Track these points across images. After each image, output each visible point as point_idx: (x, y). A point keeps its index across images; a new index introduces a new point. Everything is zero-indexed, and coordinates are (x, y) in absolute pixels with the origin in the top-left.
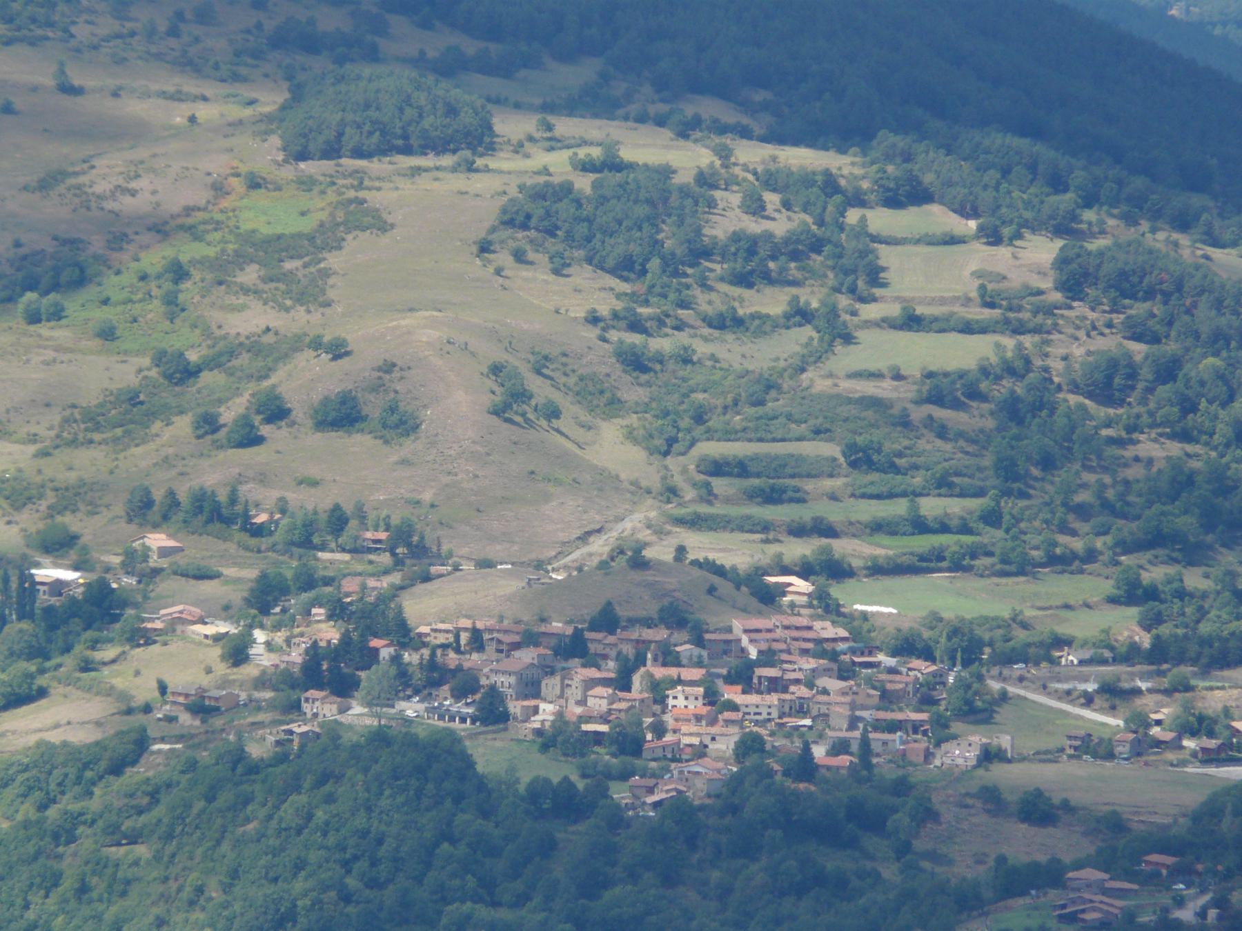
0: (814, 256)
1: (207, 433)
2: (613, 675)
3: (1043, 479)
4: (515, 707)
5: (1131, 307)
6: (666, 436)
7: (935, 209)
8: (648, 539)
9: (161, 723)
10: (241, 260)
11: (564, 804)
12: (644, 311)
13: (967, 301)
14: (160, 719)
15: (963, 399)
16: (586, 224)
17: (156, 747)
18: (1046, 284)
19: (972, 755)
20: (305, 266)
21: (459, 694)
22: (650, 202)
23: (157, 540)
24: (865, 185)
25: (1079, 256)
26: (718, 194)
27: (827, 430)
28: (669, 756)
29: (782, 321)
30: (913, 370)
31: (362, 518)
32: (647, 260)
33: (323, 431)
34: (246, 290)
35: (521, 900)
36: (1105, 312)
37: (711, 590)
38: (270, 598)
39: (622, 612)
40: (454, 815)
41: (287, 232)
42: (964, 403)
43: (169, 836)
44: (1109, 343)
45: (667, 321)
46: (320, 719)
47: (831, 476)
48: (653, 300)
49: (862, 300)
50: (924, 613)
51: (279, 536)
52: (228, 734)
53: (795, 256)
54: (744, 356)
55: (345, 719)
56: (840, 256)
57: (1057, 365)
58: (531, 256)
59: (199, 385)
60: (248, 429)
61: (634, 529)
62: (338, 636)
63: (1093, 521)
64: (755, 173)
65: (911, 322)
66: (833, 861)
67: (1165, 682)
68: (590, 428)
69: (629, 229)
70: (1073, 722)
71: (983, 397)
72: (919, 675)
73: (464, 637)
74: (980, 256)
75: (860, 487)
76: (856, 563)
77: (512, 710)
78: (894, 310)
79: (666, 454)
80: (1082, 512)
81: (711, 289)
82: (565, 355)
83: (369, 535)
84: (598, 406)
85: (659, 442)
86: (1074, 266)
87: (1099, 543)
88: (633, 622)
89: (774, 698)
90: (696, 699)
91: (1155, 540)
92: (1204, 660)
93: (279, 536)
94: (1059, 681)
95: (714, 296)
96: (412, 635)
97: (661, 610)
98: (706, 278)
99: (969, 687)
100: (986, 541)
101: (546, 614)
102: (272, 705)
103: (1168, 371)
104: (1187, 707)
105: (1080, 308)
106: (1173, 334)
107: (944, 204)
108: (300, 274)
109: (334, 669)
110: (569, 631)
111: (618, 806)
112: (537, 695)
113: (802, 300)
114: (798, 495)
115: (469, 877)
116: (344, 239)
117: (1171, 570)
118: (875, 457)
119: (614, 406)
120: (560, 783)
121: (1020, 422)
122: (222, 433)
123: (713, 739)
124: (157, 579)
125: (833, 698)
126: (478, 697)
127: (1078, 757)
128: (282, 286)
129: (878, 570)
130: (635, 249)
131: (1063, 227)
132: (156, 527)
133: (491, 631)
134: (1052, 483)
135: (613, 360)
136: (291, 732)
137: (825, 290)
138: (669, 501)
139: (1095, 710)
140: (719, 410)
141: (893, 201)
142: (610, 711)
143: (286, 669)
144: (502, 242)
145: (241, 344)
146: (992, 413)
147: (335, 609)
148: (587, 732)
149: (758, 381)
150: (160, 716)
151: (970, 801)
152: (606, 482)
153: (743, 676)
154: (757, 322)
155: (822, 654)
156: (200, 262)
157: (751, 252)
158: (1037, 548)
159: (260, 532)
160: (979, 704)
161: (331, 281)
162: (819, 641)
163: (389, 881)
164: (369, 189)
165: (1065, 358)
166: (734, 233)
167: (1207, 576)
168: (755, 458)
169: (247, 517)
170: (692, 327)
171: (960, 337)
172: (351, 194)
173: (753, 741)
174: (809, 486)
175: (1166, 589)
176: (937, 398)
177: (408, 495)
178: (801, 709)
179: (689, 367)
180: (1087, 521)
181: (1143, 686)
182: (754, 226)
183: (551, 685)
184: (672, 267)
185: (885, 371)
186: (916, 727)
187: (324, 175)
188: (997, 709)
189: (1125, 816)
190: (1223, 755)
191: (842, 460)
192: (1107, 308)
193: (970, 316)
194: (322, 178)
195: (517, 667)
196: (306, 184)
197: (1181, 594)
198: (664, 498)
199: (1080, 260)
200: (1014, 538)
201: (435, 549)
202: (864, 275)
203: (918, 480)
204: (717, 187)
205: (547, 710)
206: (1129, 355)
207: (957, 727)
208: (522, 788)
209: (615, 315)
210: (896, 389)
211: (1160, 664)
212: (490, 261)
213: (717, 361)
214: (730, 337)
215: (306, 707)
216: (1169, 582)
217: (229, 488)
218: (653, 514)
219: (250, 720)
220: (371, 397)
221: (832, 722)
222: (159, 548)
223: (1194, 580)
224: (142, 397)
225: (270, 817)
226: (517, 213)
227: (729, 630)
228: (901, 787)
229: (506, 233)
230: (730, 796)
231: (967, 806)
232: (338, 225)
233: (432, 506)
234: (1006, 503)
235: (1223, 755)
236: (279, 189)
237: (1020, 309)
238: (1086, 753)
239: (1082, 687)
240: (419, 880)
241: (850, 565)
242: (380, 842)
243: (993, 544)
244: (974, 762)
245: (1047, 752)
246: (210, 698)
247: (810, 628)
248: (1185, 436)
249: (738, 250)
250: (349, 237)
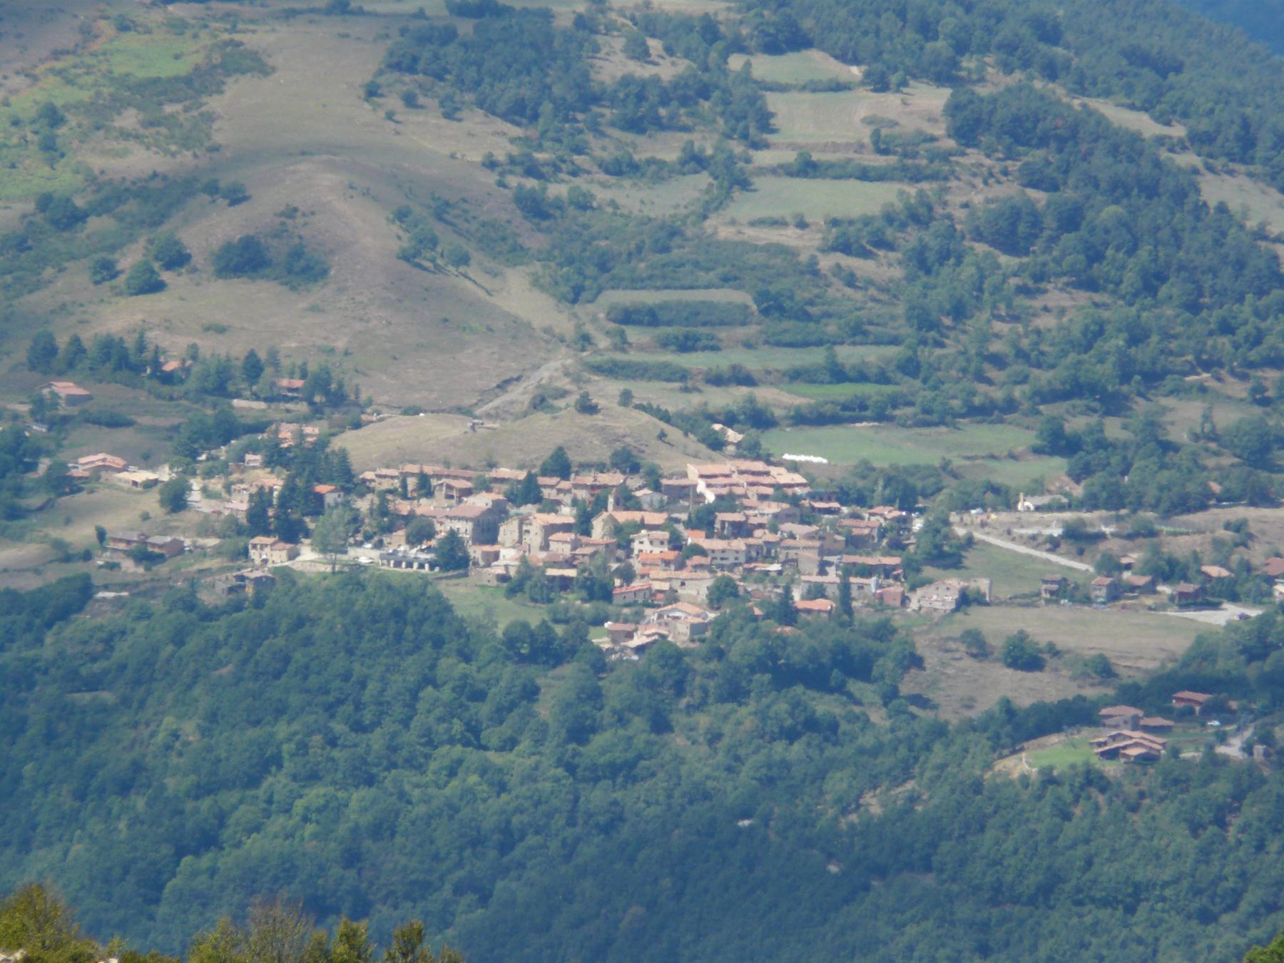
0: (701, 101)
1: (104, 279)
2: (572, 520)
3: (954, 328)
4: (476, 552)
5: (1026, 155)
6: (572, 283)
7: (815, 55)
8: (568, 387)
9: (102, 570)
10: (117, 104)
11: (543, 650)
12: (540, 156)
13: (860, 147)
14: (101, 567)
15: (869, 247)
16: (474, 68)
17: (100, 595)
18: (939, 130)
19: (951, 598)
20: (186, 110)
21: (413, 540)
22: (533, 45)
23: (65, 388)
24: (745, 31)
25: (971, 102)
26: (600, 39)
27: (736, 278)
28: (640, 601)
29: (678, 167)
30: (816, 218)
31: (275, 363)
32: (539, 104)
33: (226, 278)
34: (125, 135)
35: (509, 744)
36: (999, 159)
37: (662, 436)
38: (196, 446)
39: (574, 457)
40: (437, 659)
41: (163, 75)
42: (871, 252)
43: (137, 682)
44: (1009, 190)
45: (563, 166)
46: (270, 565)
47: (743, 324)
48: (547, 144)
49: (756, 146)
50: (855, 462)
51: (191, 384)
52: (176, 582)
53: (684, 101)
54: (642, 202)
55: (296, 565)
56: (728, 103)
57: (960, 214)
58: (421, 100)
59: (86, 232)
60: (148, 275)
61: (551, 378)
62: (281, 483)
63: (1009, 371)
64: (633, 19)
65: (807, 168)
66: (824, 705)
67: (1128, 528)
68: (496, 275)
69: (519, 73)
70: (1040, 567)
71: (890, 247)
72: (882, 520)
73: (412, 483)
74: (867, 104)
75: (773, 335)
76: (778, 413)
77: (472, 555)
78: (790, 157)
79: (574, 301)
80: (998, 361)
81: (603, 134)
82: (464, 200)
83: (285, 382)
84: (500, 253)
85: (564, 289)
86: (967, 112)
87: (1018, 392)
88: (585, 467)
89: (739, 544)
90: (662, 543)
91: (1074, 390)
92: (1165, 505)
93: (191, 384)
94: (1022, 527)
95: (606, 141)
96: (355, 480)
97: (615, 454)
98: (597, 124)
99: (938, 531)
100: (905, 390)
101: (495, 460)
102: (218, 552)
103: (1071, 220)
104: (1156, 551)
105: (974, 156)
106: (1071, 181)
107: (824, 50)
108: (181, 118)
109: (282, 517)
110: (522, 475)
111: (599, 650)
112: (493, 541)
113: (697, 145)
114: (711, 343)
115: (455, 721)
116: (223, 83)
117: (1093, 419)
118: (787, 304)
119: (516, 254)
120: (540, 627)
121: (928, 271)
122: (122, 279)
123: (683, 584)
124: (68, 426)
125: (800, 542)
126: (433, 543)
127: (1057, 602)
128: (163, 130)
129: (801, 419)
130: (526, 92)
131: (944, 75)
132: (61, 375)
133: (439, 477)
134: (964, 332)
135: (513, 206)
136: (242, 578)
137: (716, 136)
138: (583, 350)
139: (1061, 555)
140: (624, 257)
141: (773, 48)
142: (574, 557)
143: (231, 516)
144: (390, 85)
145: (126, 190)
146: (900, 263)
147: (272, 455)
148: (554, 578)
149: (661, 228)
150: (100, 563)
151: (952, 645)
152: (519, 330)
153: (704, 520)
154: (653, 168)
155: (784, 498)
156: (76, 107)
157: (641, 97)
158: (954, 397)
159: (168, 379)
160: (946, 548)
161: (216, 126)
162: (777, 487)
163: (376, 724)
164: (244, 32)
165: (966, 205)
166: (623, 78)
167: (1125, 427)
168: (664, 306)
169: (157, 365)
170: (589, 172)
171: (858, 182)
172: (226, 36)
173: (727, 585)
174: (723, 334)
175: (1088, 440)
176: (845, 247)
177: (319, 342)
178: (767, 552)
179: (589, 212)
180: (1000, 369)
181: (1108, 530)
182: (643, 71)
183: (508, 531)
184: (564, 111)
185: (789, 219)
186: (887, 572)
187: (195, 18)
188: (964, 553)
189: (1113, 661)
190: (1200, 600)
191: (754, 307)
192: (1001, 155)
193: (866, 163)
194: (192, 22)
195: (475, 513)
196: (178, 27)
197: (1102, 444)
198: (579, 346)
199: (971, 107)
200: (935, 388)
201: (352, 397)
202: (754, 122)
203: (831, 328)
204: (597, 32)
205: (508, 556)
206: (1030, 203)
207: (928, 571)
208: (500, 631)
209: (512, 160)
210: (800, 237)
211: (1117, 509)
212: (380, 106)
213: (616, 207)
214: (627, 183)
215: (254, 554)
216: (1091, 433)
217: (136, 336)
218: (569, 361)
219: (196, 567)
220: (275, 242)
221: (801, 567)
222: (68, 395)
223: (1114, 429)
224: (30, 243)
225: (245, 662)
226: (403, 55)
227: (685, 475)
228: (884, 631)
229: (392, 76)
230: (714, 642)
231: (947, 651)
232: (215, 67)
233: (346, 353)
234: (923, 352)
235: (1200, 600)
236: (149, 31)
237: (915, 155)
238: (1065, 598)
239: (1047, 532)
240: (406, 723)
241: (772, 414)
242: (363, 685)
243: (912, 395)
244: (953, 606)
245: (1025, 596)
246: (154, 545)
247: (767, 474)
248: (1091, 285)
249: (627, 96)
250: (230, 80)
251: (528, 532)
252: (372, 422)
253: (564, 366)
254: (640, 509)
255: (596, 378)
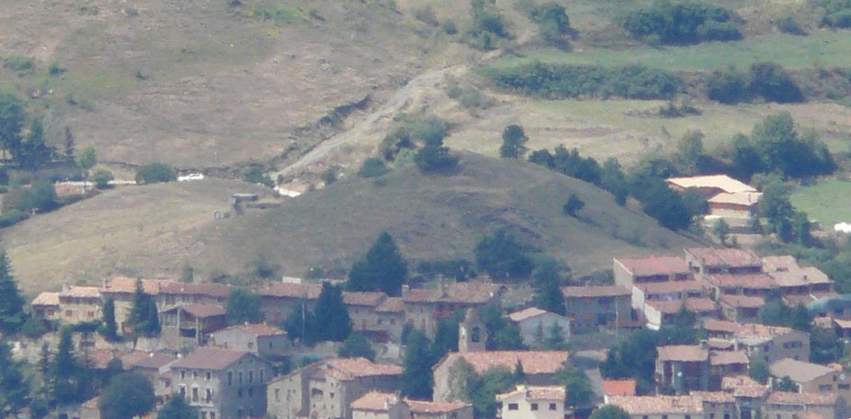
2: (396, 370)
8: (453, 117)
37: (573, 207)
39: (411, 253)
61: (426, 100)
73: (122, 310)
88: (429, 270)
96: (26, 309)
97: (482, 247)
101: (270, 263)
133: (170, 296)
138: (488, 47)
155: (780, 317)
162: (774, 294)
195: (222, 361)
198: (480, 41)
201: (61, 150)
218: (460, 71)
227: (609, 278)
233: (55, 71)
241: (825, 152)
247: (756, 270)
251: (317, 392)
252: (75, 199)
253: (450, 79)
254: (518, 346)
255: (507, 98)
